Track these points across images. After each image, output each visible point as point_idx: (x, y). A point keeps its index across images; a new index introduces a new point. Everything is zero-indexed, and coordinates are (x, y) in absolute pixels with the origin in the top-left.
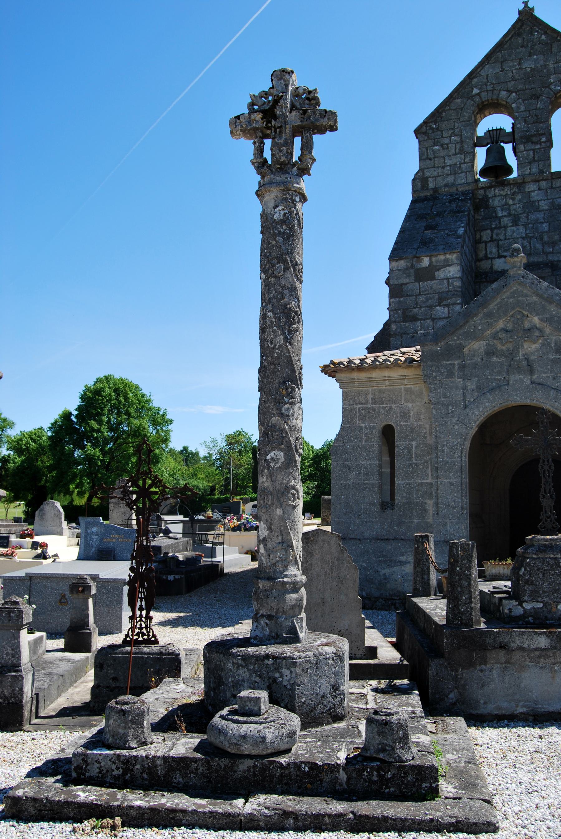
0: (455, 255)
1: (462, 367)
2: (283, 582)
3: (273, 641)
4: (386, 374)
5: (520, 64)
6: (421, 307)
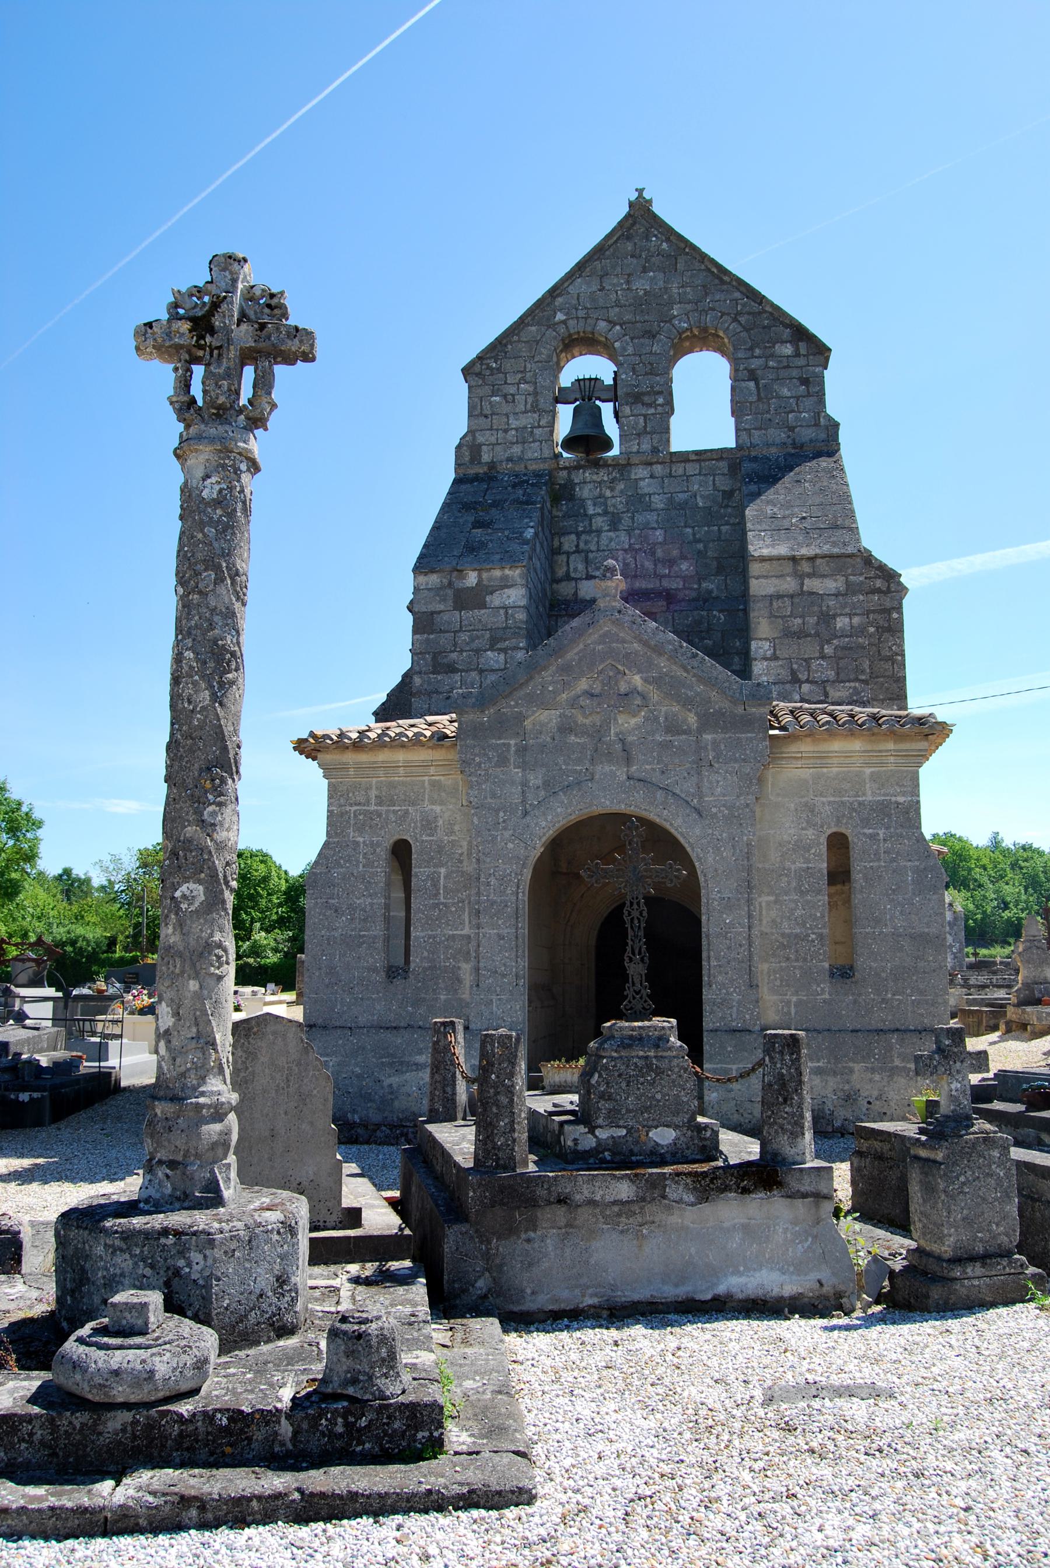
0: (518, 571)
1: (522, 750)
2: (198, 1103)
3: (177, 1205)
4: (401, 756)
5: (628, 282)
6: (462, 651)
